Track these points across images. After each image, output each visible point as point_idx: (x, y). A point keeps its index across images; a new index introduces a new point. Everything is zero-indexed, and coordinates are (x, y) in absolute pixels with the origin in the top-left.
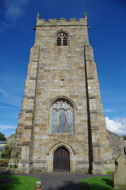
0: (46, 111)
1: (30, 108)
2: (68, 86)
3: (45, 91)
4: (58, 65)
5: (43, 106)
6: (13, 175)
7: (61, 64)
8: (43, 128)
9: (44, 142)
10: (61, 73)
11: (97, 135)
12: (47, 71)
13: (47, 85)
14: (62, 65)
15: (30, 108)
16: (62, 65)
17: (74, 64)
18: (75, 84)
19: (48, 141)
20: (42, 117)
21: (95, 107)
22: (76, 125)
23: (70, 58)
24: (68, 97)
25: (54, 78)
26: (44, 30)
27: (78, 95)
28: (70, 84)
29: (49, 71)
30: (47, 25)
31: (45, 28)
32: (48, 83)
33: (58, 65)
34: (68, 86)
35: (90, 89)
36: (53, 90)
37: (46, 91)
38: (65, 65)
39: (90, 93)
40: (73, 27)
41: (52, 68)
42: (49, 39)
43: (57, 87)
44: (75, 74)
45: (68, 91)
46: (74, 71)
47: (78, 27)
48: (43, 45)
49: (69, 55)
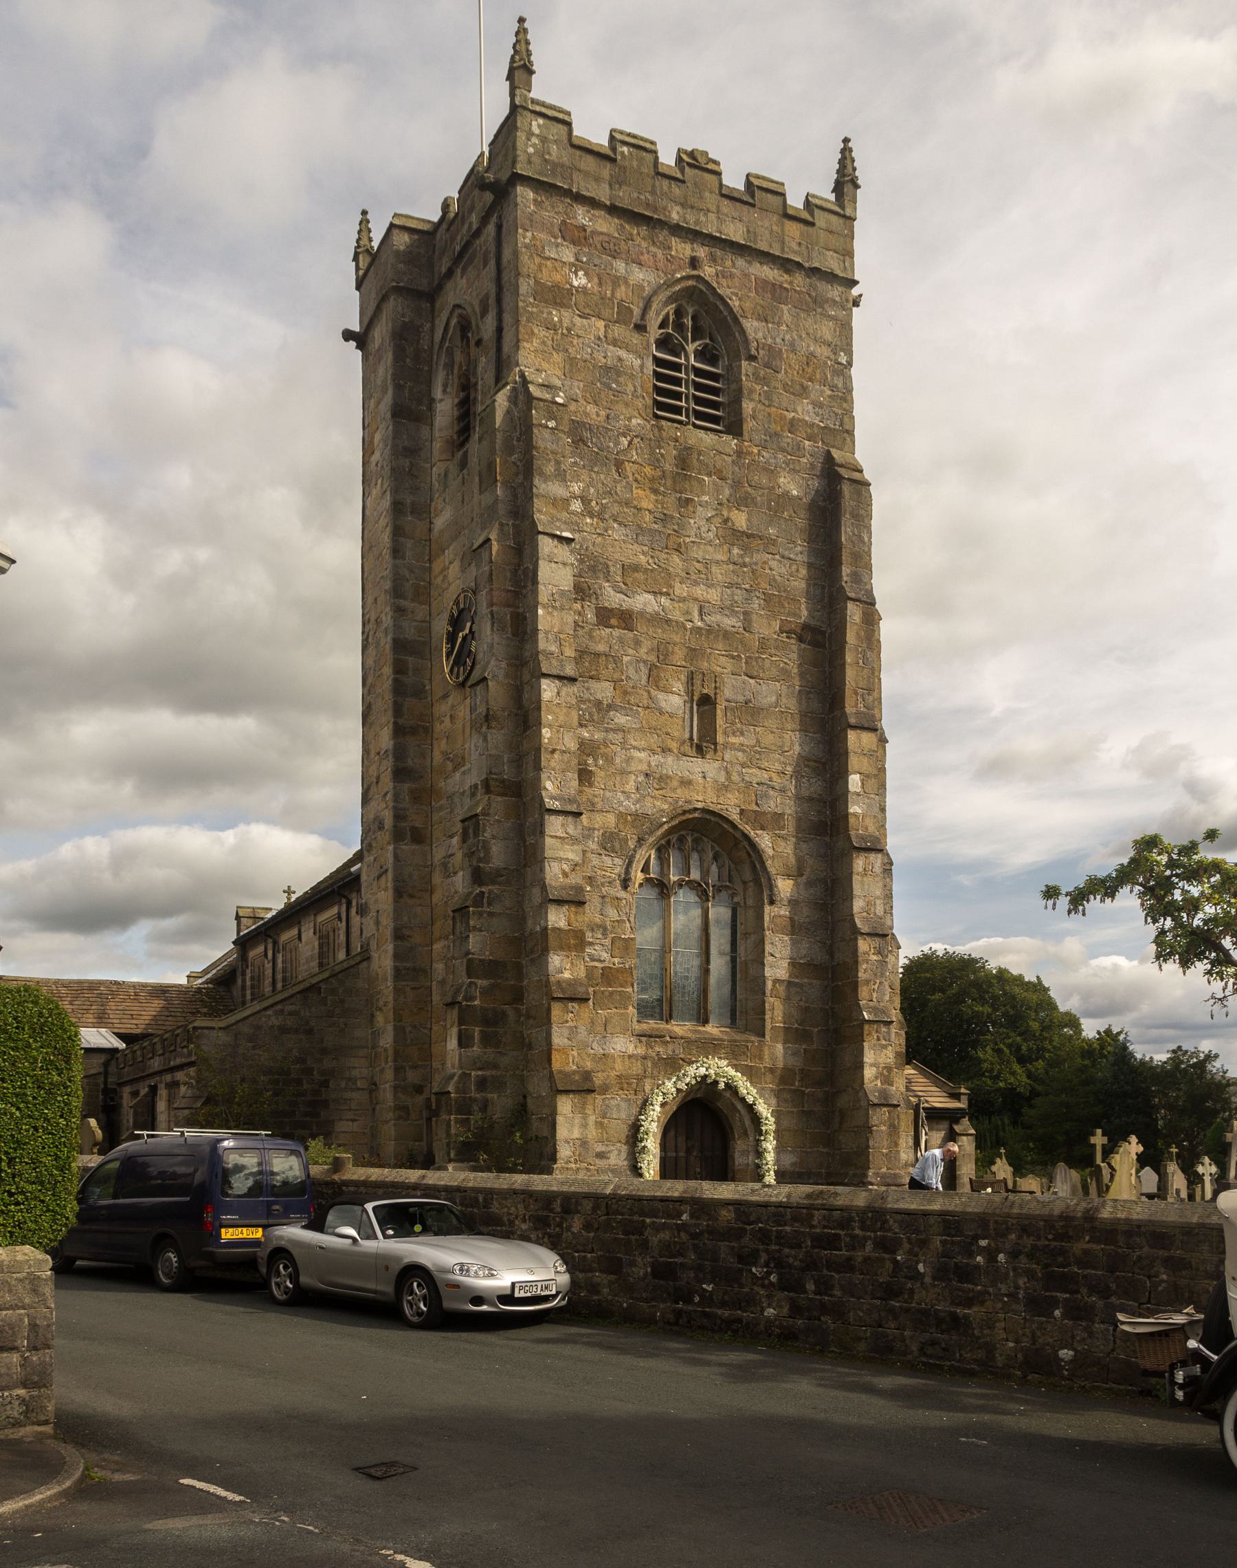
0: (622, 894)
1: (565, 875)
2: (733, 747)
3: (609, 760)
4: (680, 590)
5: (608, 861)
6: (721, 1374)
7: (696, 583)
8: (611, 994)
9: (619, 1067)
10: (693, 654)
11: (885, 1047)
12: (613, 621)
13: (621, 719)
14: (700, 591)
15: (565, 875)
16: (700, 591)
17: (768, 599)
18: (768, 739)
19: (637, 1068)
20: (605, 929)
21: (878, 902)
22: (769, 984)
23: (746, 549)
24: (734, 816)
25: (654, 676)
26: (578, 236)
27: (782, 815)
28: (742, 734)
29: (626, 619)
30: (590, 189)
31: (582, 216)
32: (627, 709)
33: (680, 590)
34: (733, 747)
35: (858, 794)
36: (655, 760)
37: (618, 760)
38: (713, 595)
39: (855, 815)
40: (769, 273)
41: (643, 601)
42: (615, 343)
43: (674, 745)
44: (774, 672)
45: (735, 777)
46: (763, 644)
47: (799, 281)
48: (577, 389)
49: (740, 519)
